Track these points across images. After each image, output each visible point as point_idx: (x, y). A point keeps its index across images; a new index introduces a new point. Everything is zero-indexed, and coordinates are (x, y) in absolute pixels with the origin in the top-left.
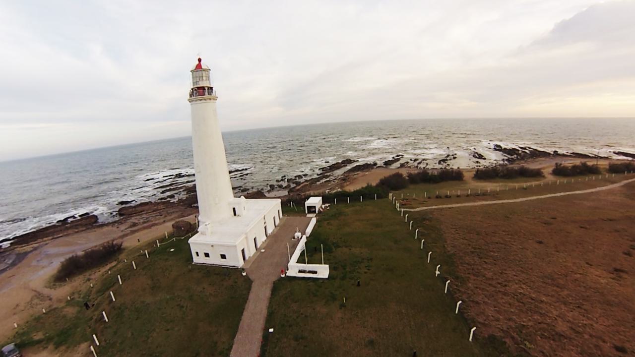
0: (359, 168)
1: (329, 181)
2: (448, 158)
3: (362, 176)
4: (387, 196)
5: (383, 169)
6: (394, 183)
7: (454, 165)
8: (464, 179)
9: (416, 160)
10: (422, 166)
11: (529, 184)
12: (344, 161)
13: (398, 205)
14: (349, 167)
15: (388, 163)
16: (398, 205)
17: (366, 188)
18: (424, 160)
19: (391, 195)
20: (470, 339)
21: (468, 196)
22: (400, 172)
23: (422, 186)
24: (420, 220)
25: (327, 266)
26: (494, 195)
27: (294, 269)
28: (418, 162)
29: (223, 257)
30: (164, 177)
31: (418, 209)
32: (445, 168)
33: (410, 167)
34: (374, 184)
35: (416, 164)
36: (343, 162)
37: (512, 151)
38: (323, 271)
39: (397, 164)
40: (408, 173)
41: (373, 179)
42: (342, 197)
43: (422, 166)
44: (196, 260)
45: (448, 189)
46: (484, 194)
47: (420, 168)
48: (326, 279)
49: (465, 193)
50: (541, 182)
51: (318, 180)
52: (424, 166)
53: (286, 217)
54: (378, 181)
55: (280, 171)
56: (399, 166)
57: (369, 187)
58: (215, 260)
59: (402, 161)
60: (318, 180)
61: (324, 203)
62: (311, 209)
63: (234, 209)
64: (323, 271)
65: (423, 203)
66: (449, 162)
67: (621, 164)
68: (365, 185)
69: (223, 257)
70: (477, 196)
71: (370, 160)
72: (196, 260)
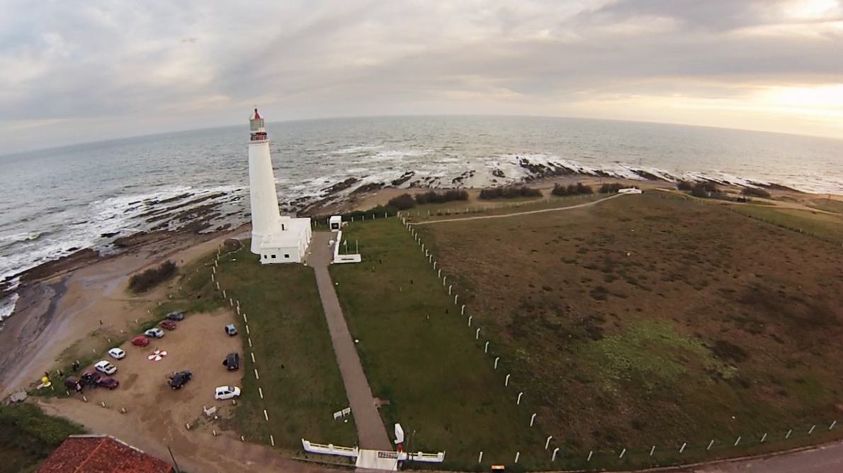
0: (364, 189)
1: (335, 203)
2: (464, 176)
3: (370, 197)
4: (396, 214)
5: (391, 189)
6: (402, 203)
7: (468, 183)
8: (469, 198)
9: (428, 178)
10: (434, 185)
11: (522, 203)
12: (347, 180)
13: (404, 220)
14: (355, 187)
15: (396, 183)
16: (404, 220)
17: (377, 208)
18: (437, 178)
19: (398, 213)
20: (546, 447)
21: (465, 213)
22: (408, 193)
23: (429, 206)
24: (419, 230)
25: (359, 255)
26: (489, 212)
27: (338, 259)
28: (430, 180)
29: (287, 256)
30: (130, 204)
31: (420, 223)
32: (458, 188)
33: (420, 187)
34: (383, 205)
35: (428, 183)
36: (346, 182)
37: (534, 168)
38: (357, 258)
39: (407, 184)
40: (416, 194)
41: (382, 199)
42: (358, 216)
43: (434, 185)
44: (263, 261)
45: (449, 208)
46: (480, 212)
47: (432, 187)
48: (359, 263)
49: (464, 211)
50: (540, 200)
51: (323, 202)
52: (436, 185)
53: (315, 232)
54: (387, 202)
55: (783, 285)
56: (409, 185)
57: (379, 207)
58: (280, 259)
59: (412, 180)
60: (323, 202)
61: (343, 220)
62: (335, 226)
63: (283, 225)
64: (357, 258)
65: (427, 219)
66: (463, 181)
67: (53, 273)
68: (375, 206)
69: (287, 256)
70: (480, 212)
71: (373, 179)
72: (263, 261)
